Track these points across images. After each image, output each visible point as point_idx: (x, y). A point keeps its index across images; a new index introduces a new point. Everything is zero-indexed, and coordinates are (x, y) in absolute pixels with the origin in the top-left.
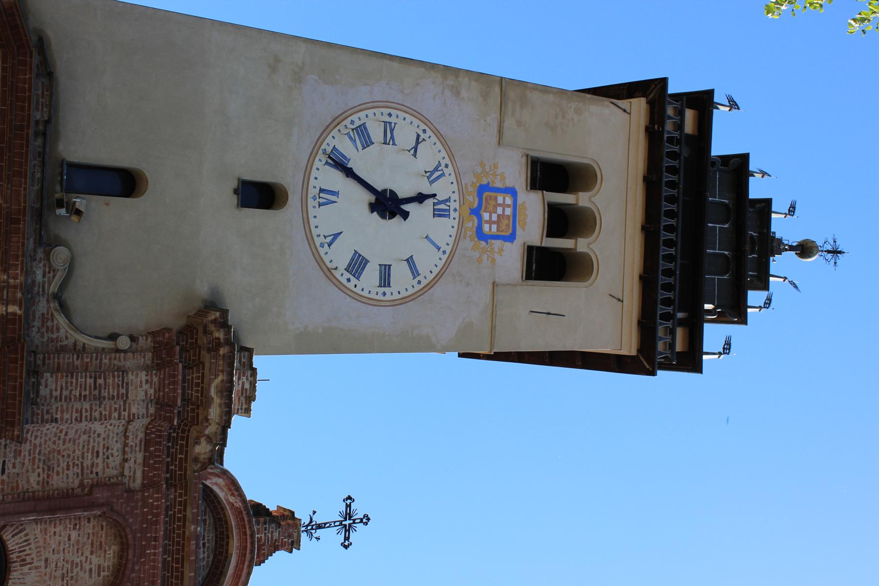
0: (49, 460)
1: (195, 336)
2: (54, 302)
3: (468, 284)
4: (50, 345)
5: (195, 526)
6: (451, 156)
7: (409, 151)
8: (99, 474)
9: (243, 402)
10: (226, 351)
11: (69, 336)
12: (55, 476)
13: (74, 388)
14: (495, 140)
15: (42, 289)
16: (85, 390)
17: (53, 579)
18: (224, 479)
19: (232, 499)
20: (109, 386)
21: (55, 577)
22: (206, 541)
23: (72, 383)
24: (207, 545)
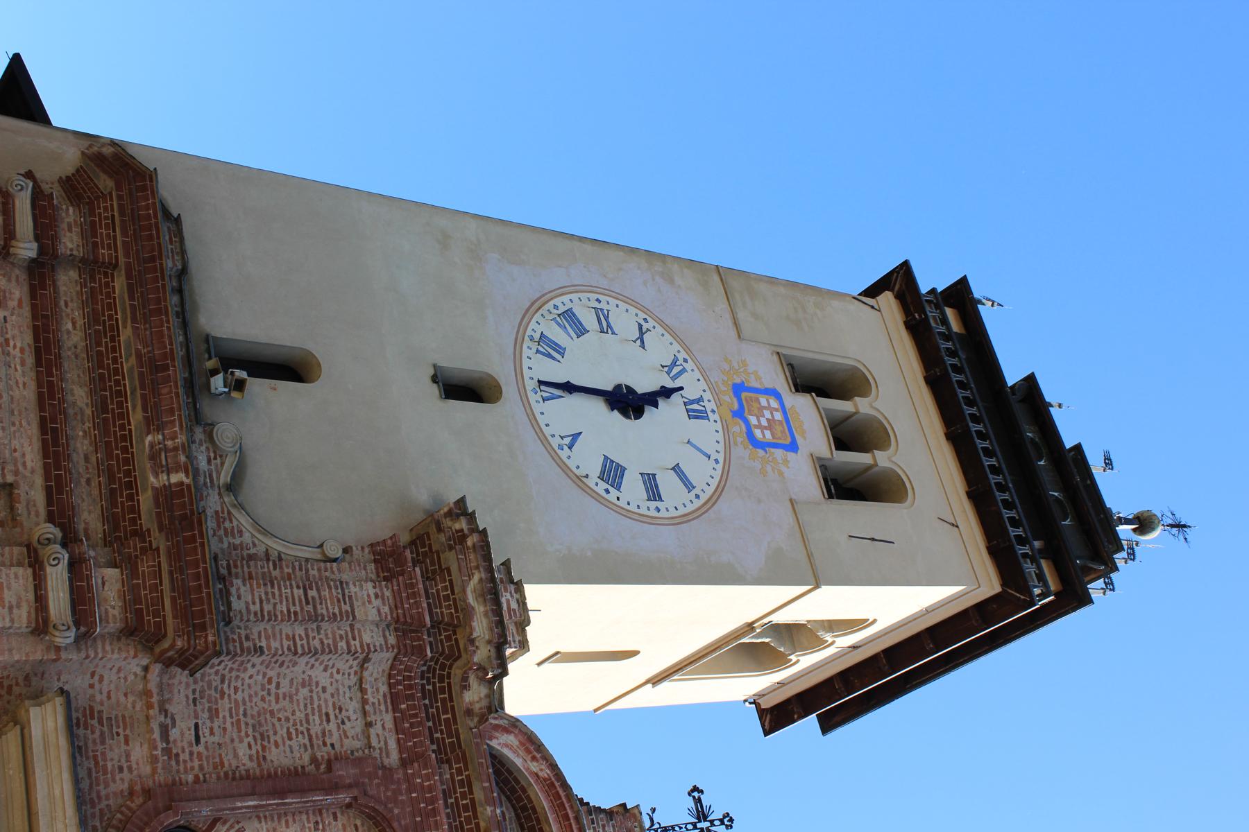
0: (260, 725)
1: (427, 543)
2: (229, 496)
3: (759, 501)
4: (234, 552)
5: (492, 808)
6: (687, 349)
7: (635, 342)
8: (336, 746)
9: (514, 631)
10: (475, 540)
11: (257, 542)
12: (273, 748)
13: (278, 601)
15: (210, 479)
16: (294, 604)
18: (516, 736)
19: (534, 766)
20: (326, 600)
23: (273, 594)
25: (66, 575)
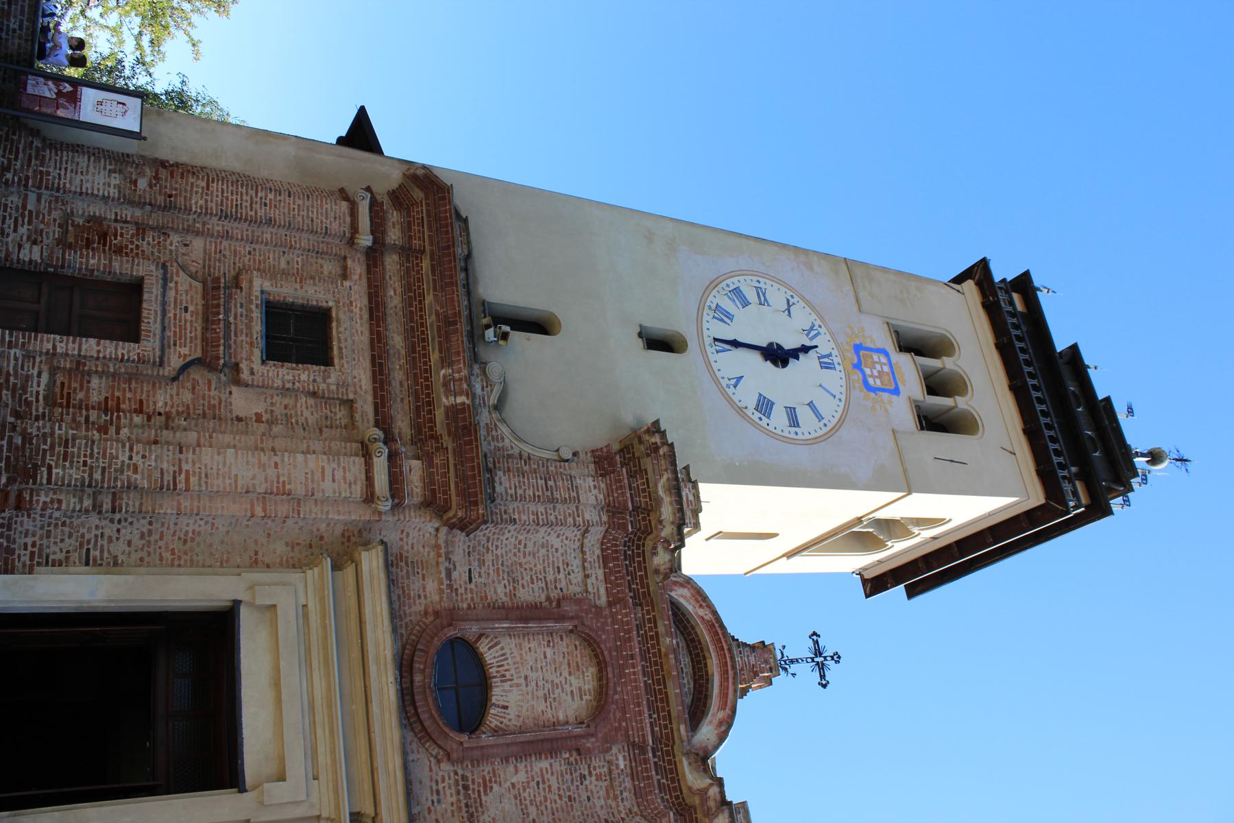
0: (513, 572)
1: (631, 451)
4: (498, 453)
6: (821, 318)
12: (521, 589)
14: (855, 308)
16: (538, 491)
17: (535, 699)
19: (701, 612)
21: (538, 697)
22: (682, 666)
23: (524, 482)
24: (685, 670)
25: (386, 464)
